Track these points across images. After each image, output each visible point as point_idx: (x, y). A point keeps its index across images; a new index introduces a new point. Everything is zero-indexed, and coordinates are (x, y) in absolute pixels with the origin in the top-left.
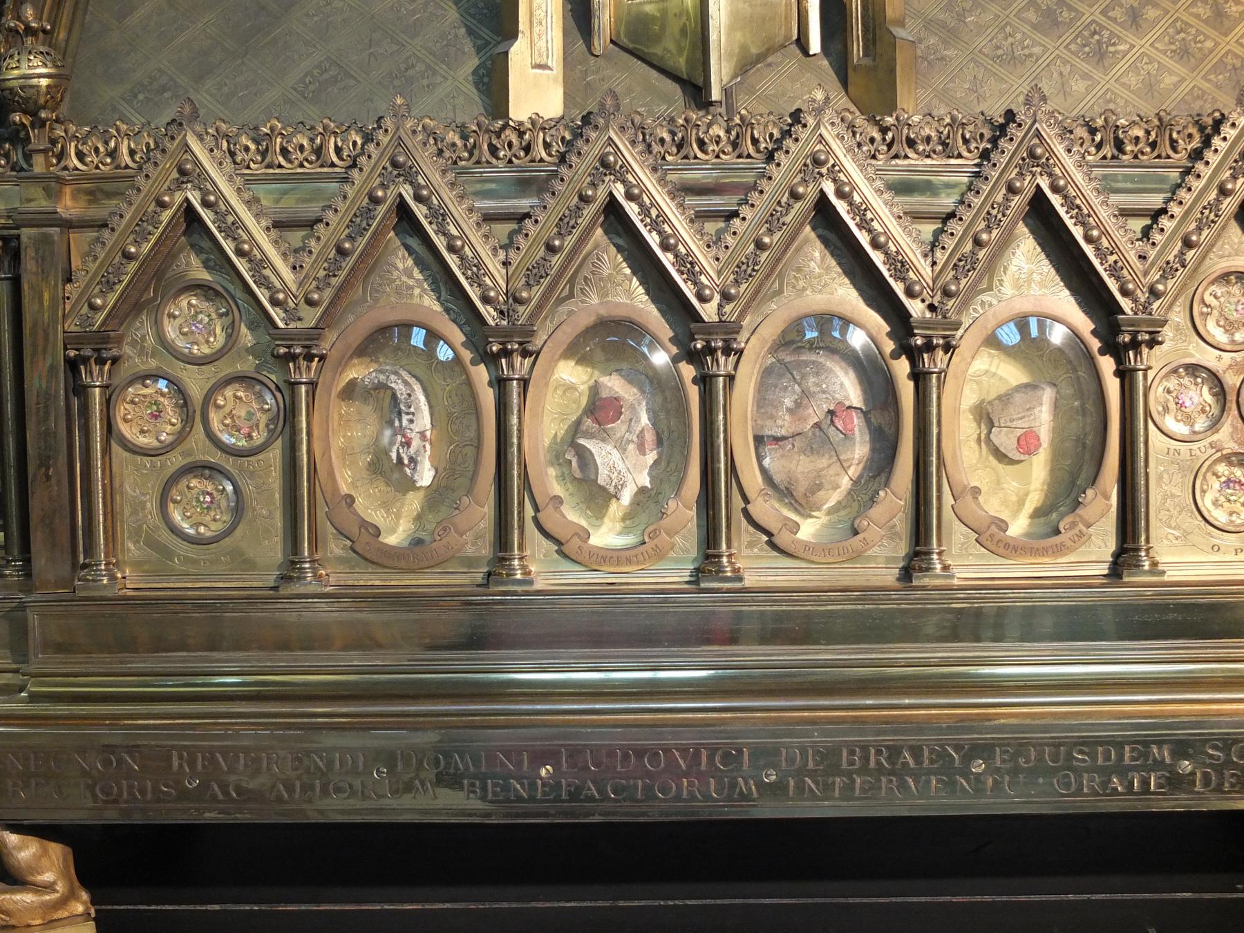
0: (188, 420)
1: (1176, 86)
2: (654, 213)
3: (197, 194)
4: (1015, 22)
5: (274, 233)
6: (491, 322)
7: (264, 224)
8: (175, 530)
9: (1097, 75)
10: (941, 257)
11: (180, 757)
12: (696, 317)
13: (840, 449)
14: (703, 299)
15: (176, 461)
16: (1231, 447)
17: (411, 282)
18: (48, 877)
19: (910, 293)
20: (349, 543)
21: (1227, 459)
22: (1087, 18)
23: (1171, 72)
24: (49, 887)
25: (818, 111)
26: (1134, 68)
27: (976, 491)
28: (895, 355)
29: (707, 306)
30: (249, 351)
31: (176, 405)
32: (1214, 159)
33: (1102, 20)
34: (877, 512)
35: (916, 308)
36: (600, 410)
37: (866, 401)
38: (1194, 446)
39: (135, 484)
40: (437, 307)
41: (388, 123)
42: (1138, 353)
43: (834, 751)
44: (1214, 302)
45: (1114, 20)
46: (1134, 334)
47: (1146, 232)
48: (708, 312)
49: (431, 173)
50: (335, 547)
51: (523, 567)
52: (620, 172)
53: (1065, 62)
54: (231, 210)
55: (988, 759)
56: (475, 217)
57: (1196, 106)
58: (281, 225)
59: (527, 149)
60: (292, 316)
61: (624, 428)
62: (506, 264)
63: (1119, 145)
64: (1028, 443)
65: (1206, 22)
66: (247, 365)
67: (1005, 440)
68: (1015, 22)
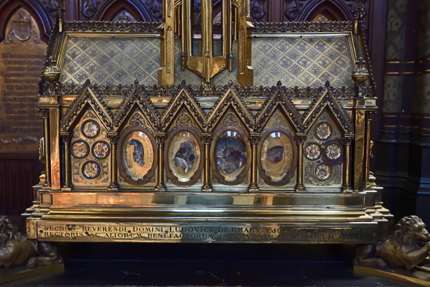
18: (52, 254)
26: (303, 76)
38: (314, 162)
45: (300, 64)
52: (186, 99)
53: (288, 74)
65: (321, 65)
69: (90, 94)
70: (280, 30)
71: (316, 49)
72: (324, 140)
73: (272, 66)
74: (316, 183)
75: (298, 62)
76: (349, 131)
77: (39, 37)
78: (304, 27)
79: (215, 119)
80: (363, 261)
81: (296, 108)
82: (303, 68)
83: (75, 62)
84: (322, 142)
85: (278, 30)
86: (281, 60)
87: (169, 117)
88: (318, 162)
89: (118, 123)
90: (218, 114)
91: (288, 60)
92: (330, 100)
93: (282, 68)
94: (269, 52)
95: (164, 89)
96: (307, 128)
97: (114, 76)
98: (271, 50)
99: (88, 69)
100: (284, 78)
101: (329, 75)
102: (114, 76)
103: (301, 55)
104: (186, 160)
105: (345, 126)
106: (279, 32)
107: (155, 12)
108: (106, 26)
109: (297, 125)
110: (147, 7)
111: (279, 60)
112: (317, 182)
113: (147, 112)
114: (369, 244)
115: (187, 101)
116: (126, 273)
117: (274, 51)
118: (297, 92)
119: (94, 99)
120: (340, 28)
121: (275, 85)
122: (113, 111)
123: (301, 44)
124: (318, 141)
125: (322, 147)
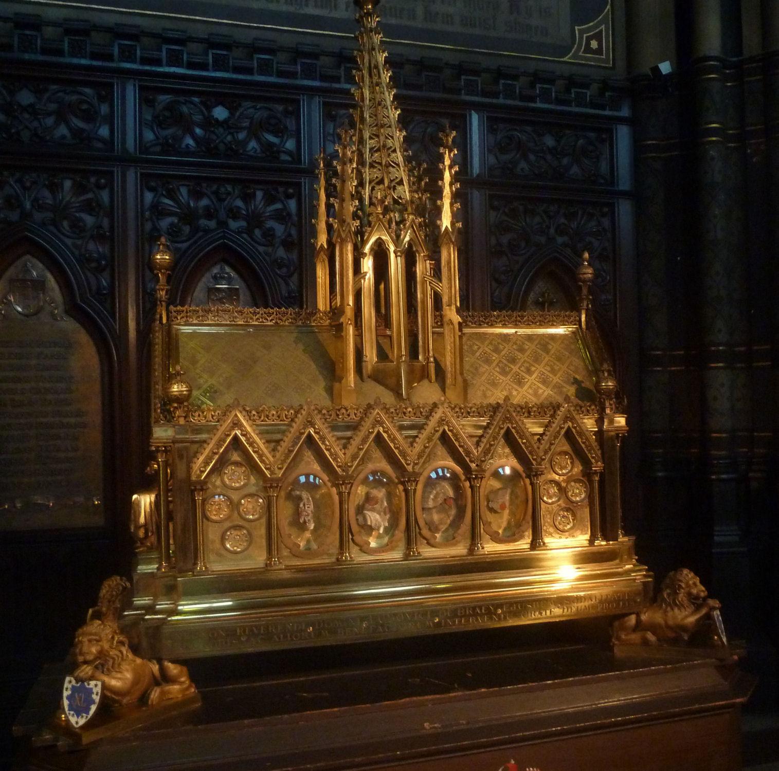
0: (232, 510)
1: (543, 393)
2: (392, 437)
3: (240, 431)
4: (493, 371)
5: (266, 444)
6: (340, 474)
7: (263, 441)
8: (227, 549)
9: (520, 389)
10: (480, 449)
11: (240, 629)
12: (405, 470)
13: (546, 527)
14: (408, 464)
15: (227, 524)
16: (563, 505)
17: (310, 460)
18: (183, 679)
19: (472, 462)
20: (289, 550)
21: (562, 510)
22: (514, 371)
23: (541, 389)
24: (183, 682)
25: (442, 404)
26: (530, 387)
27: (490, 523)
28: (465, 480)
29: (409, 466)
30: (254, 485)
31: (227, 505)
32: (558, 418)
33: (518, 370)
34: (460, 531)
35: (473, 466)
36: (368, 498)
37: (455, 495)
38: (553, 506)
39: (212, 534)
40: (319, 468)
41: (305, 407)
42: (537, 478)
43: (456, 610)
44: (557, 461)
45: (522, 371)
46: (536, 472)
47: (539, 440)
48: (410, 468)
49: (319, 424)
50: (285, 553)
51: (350, 556)
52: (380, 423)
53: (510, 385)
54: (251, 437)
55: (502, 608)
56: (334, 439)
57: (550, 399)
58: (268, 442)
59: (349, 415)
60: (272, 473)
61: (379, 507)
62: (345, 454)
63: (529, 413)
64: (503, 507)
65: (549, 372)
66: (253, 490)
67: (495, 506)
68: (493, 371)
69: (239, 421)
70: (487, 323)
71: (537, 350)
72: (563, 475)
73: (486, 375)
74: (558, 536)
75: (519, 369)
76: (597, 462)
77: (61, 308)
78: (519, 318)
79: (423, 451)
80: (626, 637)
81: (530, 432)
82: (527, 376)
83: (198, 371)
84: (562, 478)
85: (484, 323)
86: (497, 365)
87: (358, 453)
88: (558, 505)
89: (282, 464)
90: (493, 443)
91: (506, 365)
92: (572, 419)
93: (501, 377)
94: (478, 354)
95: (347, 410)
96: (351, 466)
97: (265, 392)
98: (481, 350)
99: (222, 381)
100: (506, 390)
101: (563, 387)
102: (265, 392)
103: (521, 358)
104: (380, 514)
105: (591, 454)
106: (486, 325)
107: (280, 268)
108: (236, 314)
109: (532, 455)
110: (77, 253)
111: (494, 364)
112: (558, 533)
113: (326, 445)
114: (631, 614)
115: (383, 427)
116: (305, 695)
117: (485, 353)
118: (526, 410)
119: (245, 427)
120: (516, 321)
121: (501, 402)
122: (195, 446)
123: (494, 342)
124: (557, 477)
125: (564, 485)
